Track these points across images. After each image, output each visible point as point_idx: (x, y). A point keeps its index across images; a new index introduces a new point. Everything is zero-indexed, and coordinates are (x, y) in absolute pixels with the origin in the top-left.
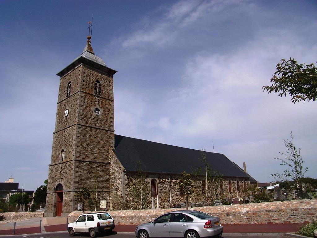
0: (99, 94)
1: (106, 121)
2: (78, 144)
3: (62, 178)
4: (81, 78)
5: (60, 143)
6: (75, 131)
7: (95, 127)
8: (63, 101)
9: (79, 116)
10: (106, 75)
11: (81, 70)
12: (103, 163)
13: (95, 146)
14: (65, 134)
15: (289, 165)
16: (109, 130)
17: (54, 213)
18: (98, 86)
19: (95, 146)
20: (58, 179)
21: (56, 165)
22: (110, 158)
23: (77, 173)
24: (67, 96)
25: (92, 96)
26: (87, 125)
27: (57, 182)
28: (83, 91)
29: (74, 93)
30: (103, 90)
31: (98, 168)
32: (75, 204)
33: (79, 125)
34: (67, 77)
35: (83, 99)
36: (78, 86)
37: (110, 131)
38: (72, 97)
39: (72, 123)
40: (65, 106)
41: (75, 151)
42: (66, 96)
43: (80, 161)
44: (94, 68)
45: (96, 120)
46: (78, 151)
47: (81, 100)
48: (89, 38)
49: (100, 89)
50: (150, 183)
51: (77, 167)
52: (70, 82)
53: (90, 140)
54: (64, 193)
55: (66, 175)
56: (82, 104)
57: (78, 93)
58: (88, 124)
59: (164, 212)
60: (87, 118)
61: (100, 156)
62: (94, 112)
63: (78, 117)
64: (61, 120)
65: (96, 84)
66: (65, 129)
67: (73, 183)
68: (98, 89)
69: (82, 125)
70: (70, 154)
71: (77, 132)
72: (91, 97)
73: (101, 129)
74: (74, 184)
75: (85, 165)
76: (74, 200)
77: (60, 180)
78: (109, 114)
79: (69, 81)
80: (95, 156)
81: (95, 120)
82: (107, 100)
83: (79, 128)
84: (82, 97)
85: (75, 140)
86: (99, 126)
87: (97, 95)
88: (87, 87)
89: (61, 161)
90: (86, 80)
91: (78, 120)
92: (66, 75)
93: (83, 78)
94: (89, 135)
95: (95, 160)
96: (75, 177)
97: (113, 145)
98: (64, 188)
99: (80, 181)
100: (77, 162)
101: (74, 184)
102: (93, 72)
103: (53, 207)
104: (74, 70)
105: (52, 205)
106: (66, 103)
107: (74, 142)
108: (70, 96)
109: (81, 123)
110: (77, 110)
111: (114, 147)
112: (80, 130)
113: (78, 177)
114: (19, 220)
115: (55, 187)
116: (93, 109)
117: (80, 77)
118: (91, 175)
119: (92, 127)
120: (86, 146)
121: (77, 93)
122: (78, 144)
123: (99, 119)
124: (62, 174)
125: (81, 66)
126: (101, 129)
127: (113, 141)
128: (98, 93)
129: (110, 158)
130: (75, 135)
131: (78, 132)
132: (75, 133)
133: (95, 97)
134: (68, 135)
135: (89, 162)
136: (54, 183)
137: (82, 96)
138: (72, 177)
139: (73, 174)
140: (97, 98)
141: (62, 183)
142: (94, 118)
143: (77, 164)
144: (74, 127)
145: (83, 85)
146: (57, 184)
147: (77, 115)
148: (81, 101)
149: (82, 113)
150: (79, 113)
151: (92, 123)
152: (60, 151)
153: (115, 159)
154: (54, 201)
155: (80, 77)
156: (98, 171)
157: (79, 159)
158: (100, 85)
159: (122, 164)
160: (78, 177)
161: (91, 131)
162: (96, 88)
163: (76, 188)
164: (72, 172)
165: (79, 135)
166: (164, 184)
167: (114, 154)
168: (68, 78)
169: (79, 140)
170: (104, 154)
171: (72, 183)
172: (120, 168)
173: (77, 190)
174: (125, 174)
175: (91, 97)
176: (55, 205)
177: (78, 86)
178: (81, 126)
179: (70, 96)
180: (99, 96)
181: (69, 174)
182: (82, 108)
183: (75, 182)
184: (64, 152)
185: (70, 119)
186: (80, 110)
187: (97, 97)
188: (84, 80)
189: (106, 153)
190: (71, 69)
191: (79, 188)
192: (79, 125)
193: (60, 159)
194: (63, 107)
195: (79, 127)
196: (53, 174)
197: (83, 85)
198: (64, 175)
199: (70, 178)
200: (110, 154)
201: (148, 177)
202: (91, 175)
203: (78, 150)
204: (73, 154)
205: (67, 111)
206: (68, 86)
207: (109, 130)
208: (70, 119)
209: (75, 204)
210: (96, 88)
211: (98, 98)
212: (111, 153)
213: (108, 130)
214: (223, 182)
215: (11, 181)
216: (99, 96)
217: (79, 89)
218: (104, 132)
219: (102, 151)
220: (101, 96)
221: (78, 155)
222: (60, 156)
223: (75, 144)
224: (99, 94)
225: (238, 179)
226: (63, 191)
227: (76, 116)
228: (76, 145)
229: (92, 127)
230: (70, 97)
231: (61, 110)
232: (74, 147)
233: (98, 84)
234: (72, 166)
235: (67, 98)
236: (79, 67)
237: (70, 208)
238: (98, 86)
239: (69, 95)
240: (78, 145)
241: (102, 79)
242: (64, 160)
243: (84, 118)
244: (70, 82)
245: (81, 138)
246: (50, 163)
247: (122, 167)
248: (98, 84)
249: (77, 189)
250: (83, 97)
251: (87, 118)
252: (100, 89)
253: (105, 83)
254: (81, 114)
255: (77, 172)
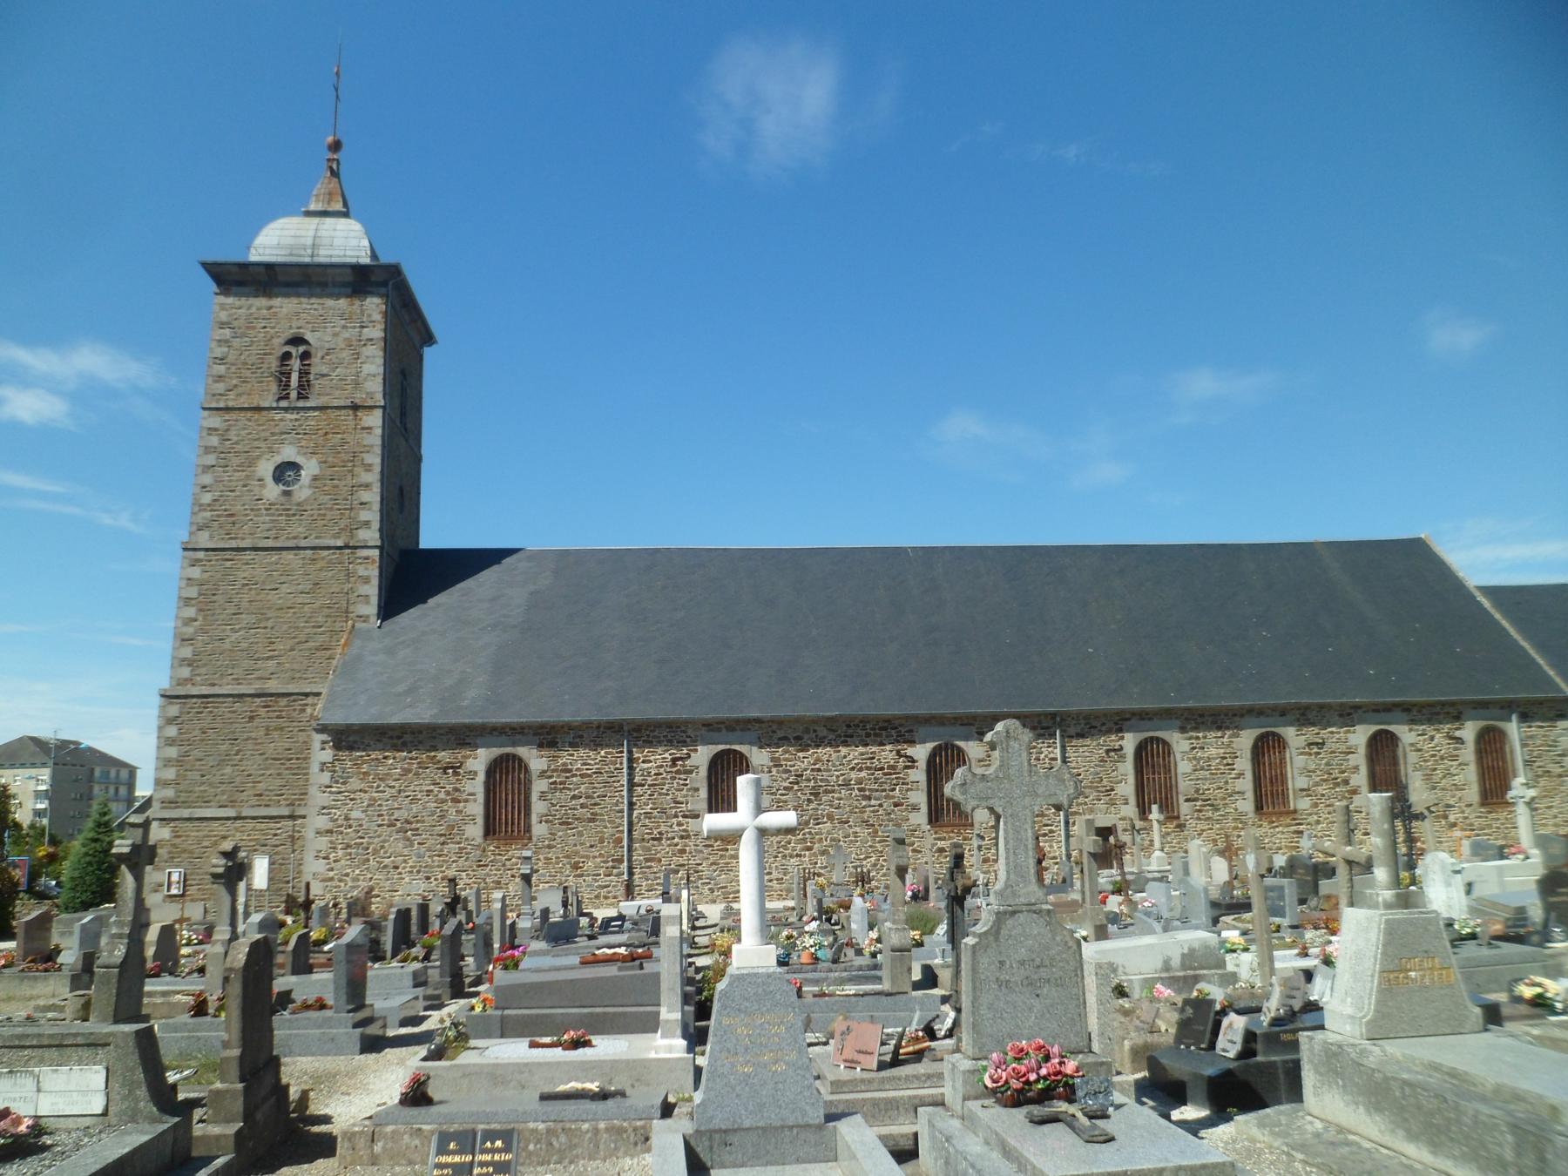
0: (300, 397)
15: (1236, 1093)
16: (347, 547)
18: (295, 364)
19: (269, 624)
26: (234, 544)
43: (186, 697)
46: (184, 660)
48: (336, 146)
53: (245, 604)
61: (295, 666)
69: (207, 550)
71: (184, 582)
83: (194, 563)
109: (204, 539)
116: (266, 468)
128: (294, 395)
166: (582, 776)
170: (318, 654)
178: (201, 555)
203: (187, 652)
207: (347, 547)
210: (283, 377)
219: (311, 644)
221: (185, 672)
238: (295, 364)
246: (165, 683)
252: (304, 373)
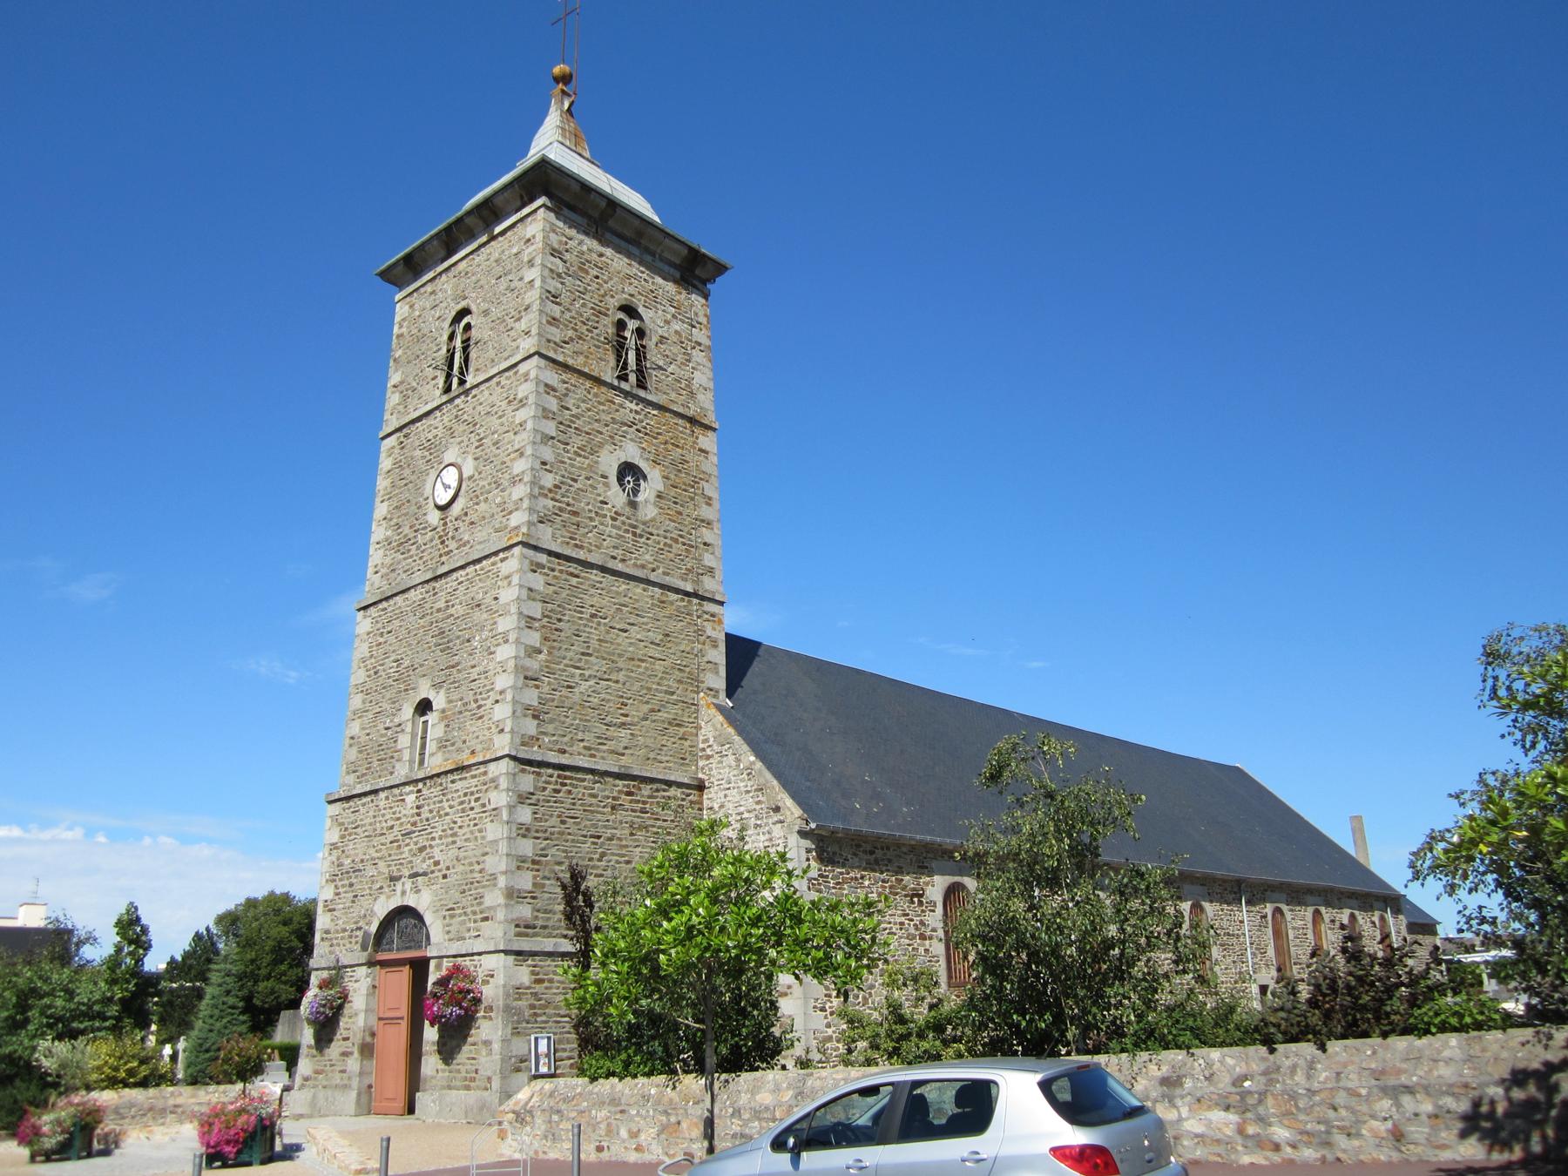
0: (641, 385)
1: (676, 541)
2: (528, 663)
3: (415, 875)
4: (538, 283)
5: (407, 663)
6: (510, 583)
7: (620, 567)
8: (419, 419)
9: (532, 496)
10: (675, 282)
11: (539, 237)
12: (669, 784)
13: (621, 676)
14: (442, 604)
17: (359, 1094)
18: (631, 341)
19: (621, 676)
20: (394, 879)
21: (375, 792)
22: (708, 757)
23: (524, 836)
24: (448, 390)
25: (604, 389)
26: (581, 555)
27: (383, 897)
28: (551, 354)
29: (495, 371)
30: (661, 363)
31: (643, 811)
32: (516, 1032)
33: (536, 548)
34: (447, 285)
35: (553, 404)
36: (523, 325)
37: (703, 598)
38: (483, 394)
39: (484, 539)
40: (433, 449)
41: (515, 702)
42: (438, 393)
44: (608, 235)
45: (627, 531)
47: (544, 409)
49: (641, 354)
50: (939, 909)
51: (523, 798)
52: (465, 312)
53: (594, 644)
54: (433, 963)
55: (453, 852)
56: (550, 428)
57: (523, 368)
58: (581, 547)
59: (1446, 1045)
60: (575, 513)
61: (649, 742)
62: (613, 479)
63: (526, 504)
64: (406, 530)
65: (621, 325)
66: (436, 578)
67: (501, 900)
68: (632, 357)
70: (472, 726)
71: (525, 592)
72: (596, 395)
73: (654, 584)
74: (506, 906)
75: (570, 792)
76: (507, 1009)
77: (408, 885)
78: (692, 499)
79: (459, 307)
80: (625, 742)
81: (619, 528)
82: (681, 422)
83: (536, 568)
84: (550, 388)
85: (512, 637)
86: (643, 567)
87: (624, 386)
88: (570, 333)
89: (411, 769)
90: (565, 298)
91: (530, 524)
92: (440, 274)
93: (554, 285)
94: (593, 616)
95: (625, 760)
96: (515, 864)
97: (720, 683)
98: (435, 926)
99: (543, 886)
100: (523, 771)
101: (506, 906)
102: (601, 255)
103: (356, 1054)
104: (493, 238)
105: (348, 1043)
106: (440, 432)
107: (506, 652)
108: (468, 385)
109: (547, 537)
110: (520, 466)
111: (722, 695)
112: (538, 581)
113: (534, 862)
114: (142, 1136)
115: (373, 929)
116: (609, 462)
117: (533, 274)
118: (603, 855)
119: (603, 569)
120: (573, 676)
121: (516, 365)
122: (528, 663)
123: (644, 523)
124: (422, 849)
125: (535, 211)
126: (654, 584)
127: (719, 656)
128: (633, 378)
129: (708, 757)
130: (513, 609)
131: (530, 590)
132: (508, 595)
133: (618, 400)
134: (458, 610)
135: (592, 771)
136: (365, 903)
137: (546, 385)
138: (497, 863)
139: (503, 847)
140: (628, 404)
141: (422, 901)
142: (614, 519)
143: (527, 781)
144: (502, 560)
145: (553, 321)
146: (382, 908)
147: (520, 491)
148: (546, 414)
149: (548, 480)
150: (533, 483)
151: (601, 545)
152: (408, 711)
153: (738, 761)
154: (362, 1017)
155: (533, 274)
156: (640, 828)
157: (535, 753)
158: (640, 333)
159: (786, 785)
160: (534, 862)
161: (600, 593)
162: (620, 348)
163: (519, 935)
164: (495, 831)
165: (536, 610)
167: (731, 730)
168: (449, 288)
169: (534, 638)
171: (494, 898)
172: (777, 809)
173: (525, 945)
174: (808, 851)
175: (596, 395)
176: (368, 1039)
177: (523, 325)
178: (543, 558)
179: (468, 385)
180: (642, 393)
181: (471, 845)
182: (547, 453)
183: (513, 895)
184: (431, 718)
185: (473, 517)
186: (538, 466)
187: (627, 394)
188: (554, 297)
189: (681, 727)
190: (472, 236)
191: (535, 935)
192: (536, 548)
193: (406, 756)
194: (418, 453)
195: (532, 562)
196: (358, 849)
197: (553, 321)
198: (436, 851)
199: (477, 868)
200: (707, 731)
201: (923, 868)
202: (603, 855)
204: (499, 726)
205: (451, 476)
206: (451, 337)
207: (695, 595)
208: (473, 517)
209: (516, 1032)
210: (620, 348)
211: (633, 406)
212: (712, 725)
213: (689, 588)
214: (1289, 916)
215: (31, 918)
216: (642, 393)
217: (528, 345)
218: (672, 603)
220: (650, 397)
221: (531, 727)
222: (404, 741)
223: (512, 663)
224: (641, 385)
225: (1354, 902)
226: (429, 955)
227: (515, 497)
228: (518, 669)
229: (603, 569)
230: (466, 392)
231: (407, 472)
232: (504, 681)
233: (632, 325)
234: (493, 795)
235: (451, 401)
236: (521, 220)
237: (483, 1060)
238: (631, 341)
239: (462, 382)
240: (527, 669)
241: (653, 299)
242: (435, 763)
243: (561, 509)
244: (465, 312)
245: (548, 622)
247: (792, 810)
248: (632, 325)
249: (527, 935)
250: (554, 390)
251: (575, 513)
253: (667, 322)
254: (541, 487)
255: (525, 831)
